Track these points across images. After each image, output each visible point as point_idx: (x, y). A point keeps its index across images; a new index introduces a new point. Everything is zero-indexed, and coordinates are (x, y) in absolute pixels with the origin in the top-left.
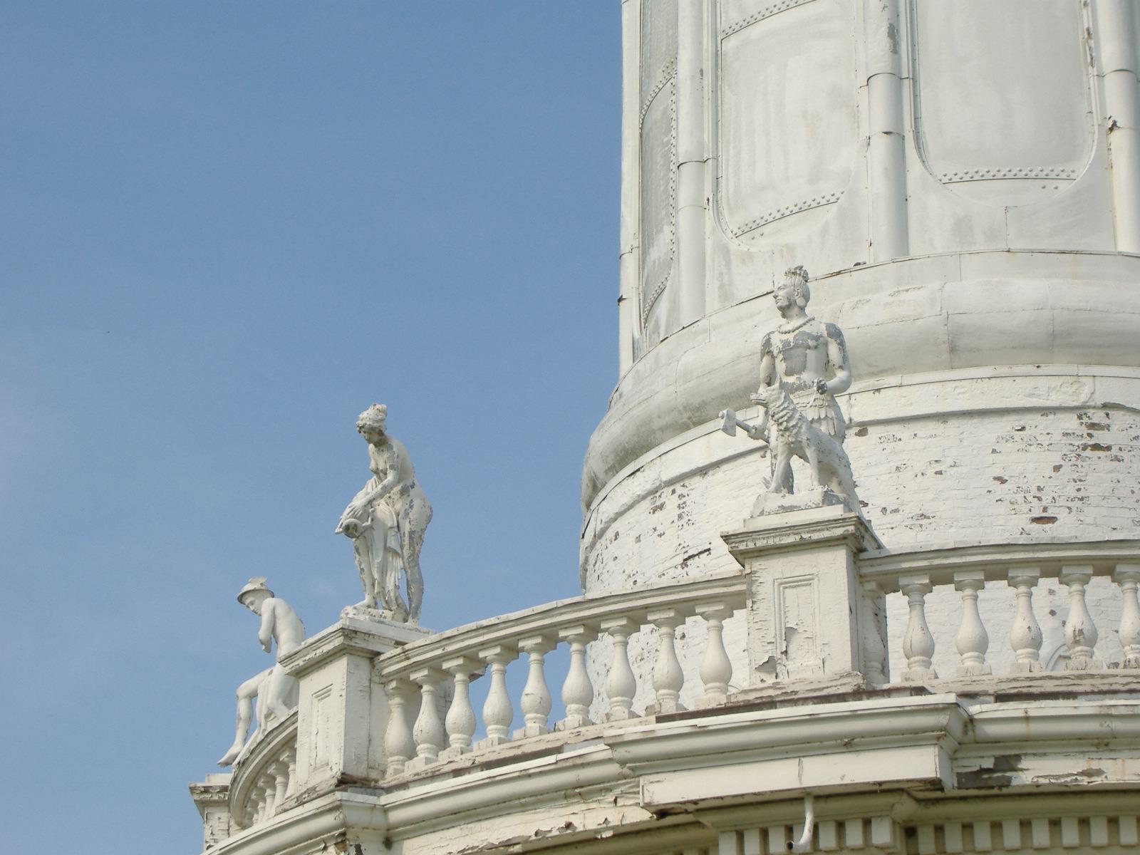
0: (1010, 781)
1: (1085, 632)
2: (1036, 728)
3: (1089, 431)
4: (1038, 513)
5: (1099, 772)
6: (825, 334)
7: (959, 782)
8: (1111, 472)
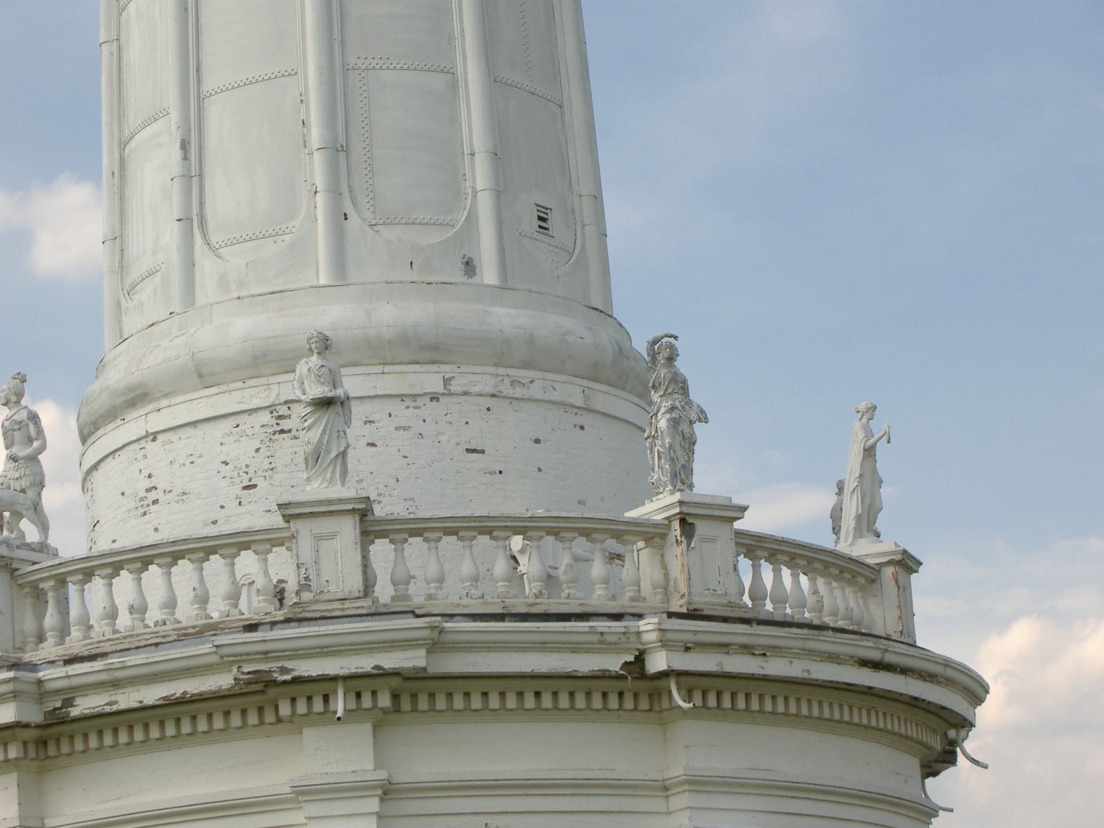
0: (69, 714)
1: (134, 606)
2: (76, 682)
3: (278, 421)
4: (246, 483)
5: (116, 702)
6: (26, 419)
7: (45, 717)
8: (291, 447)
